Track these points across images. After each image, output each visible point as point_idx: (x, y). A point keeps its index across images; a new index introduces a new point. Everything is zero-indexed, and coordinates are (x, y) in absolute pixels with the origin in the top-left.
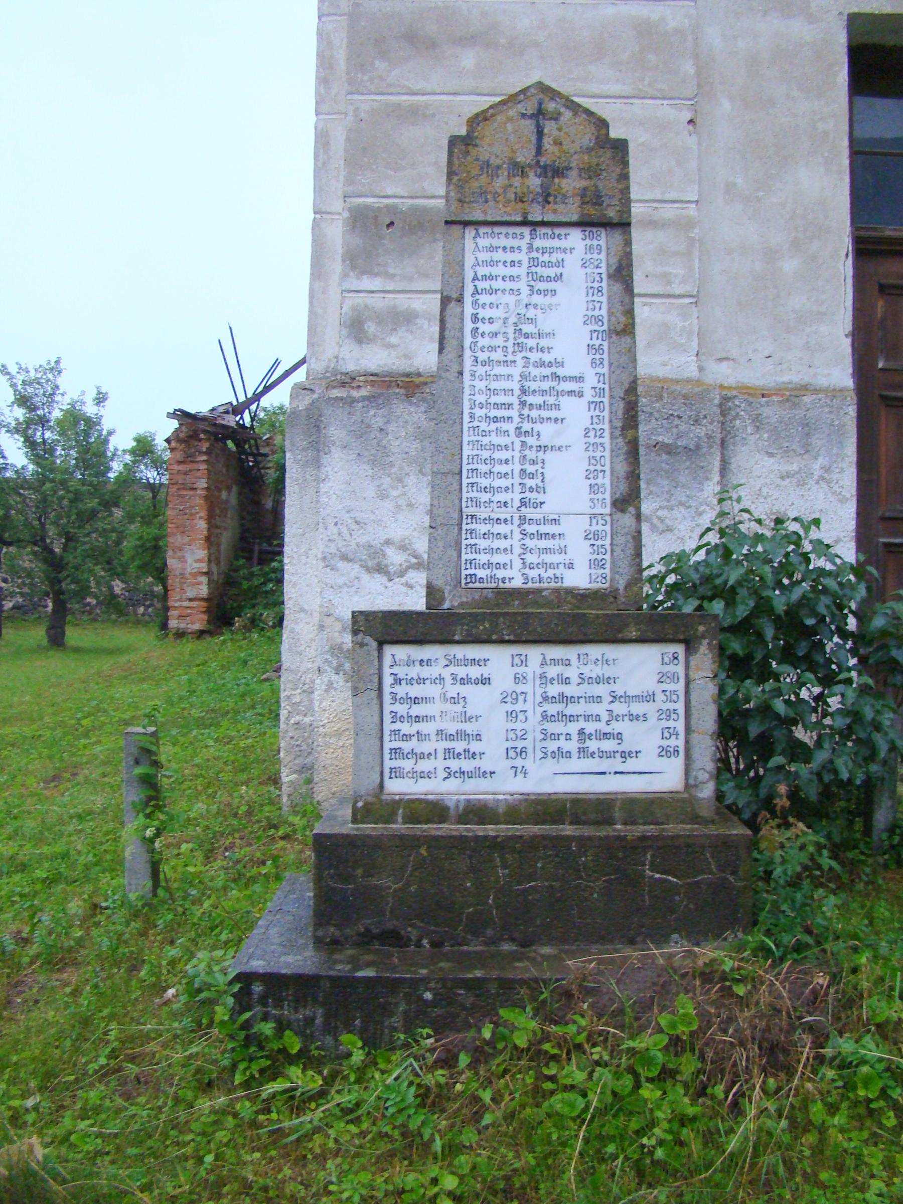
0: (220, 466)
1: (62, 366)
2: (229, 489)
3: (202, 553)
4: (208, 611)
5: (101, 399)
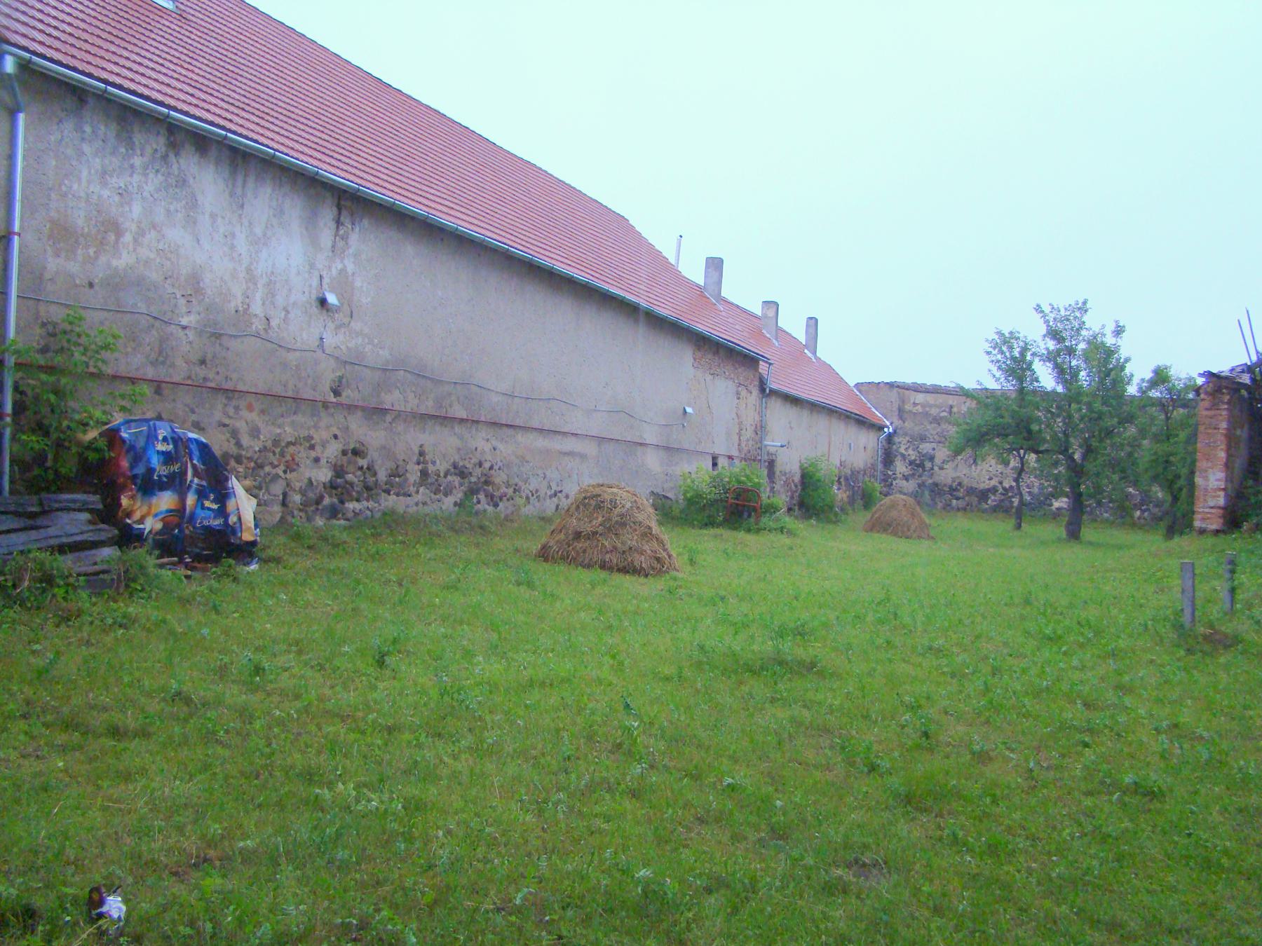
0: (1236, 412)
1: (1088, 306)
2: (1242, 428)
3: (1221, 475)
4: (1224, 516)
5: (1119, 331)
